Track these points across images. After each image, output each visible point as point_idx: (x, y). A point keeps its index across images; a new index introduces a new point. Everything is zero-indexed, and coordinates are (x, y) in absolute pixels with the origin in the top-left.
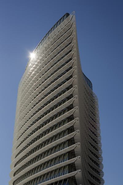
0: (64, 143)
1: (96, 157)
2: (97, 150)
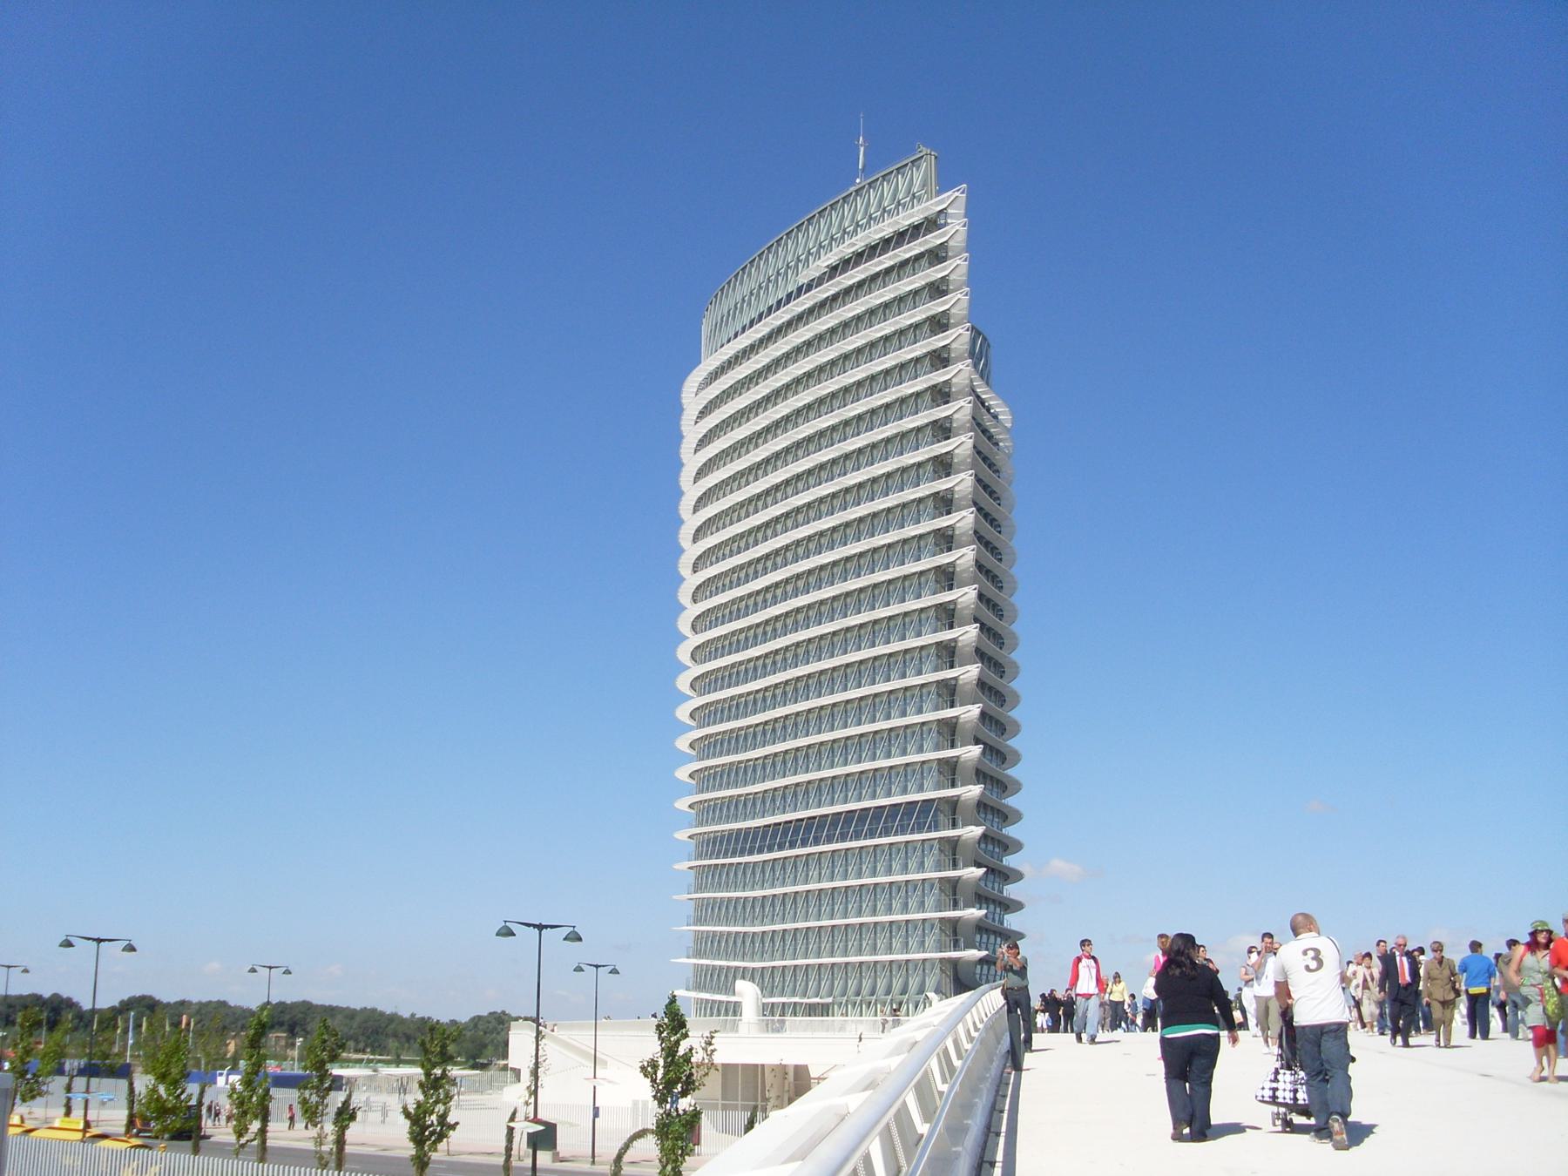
0: (916, 293)
1: (990, 467)
2: (997, 471)
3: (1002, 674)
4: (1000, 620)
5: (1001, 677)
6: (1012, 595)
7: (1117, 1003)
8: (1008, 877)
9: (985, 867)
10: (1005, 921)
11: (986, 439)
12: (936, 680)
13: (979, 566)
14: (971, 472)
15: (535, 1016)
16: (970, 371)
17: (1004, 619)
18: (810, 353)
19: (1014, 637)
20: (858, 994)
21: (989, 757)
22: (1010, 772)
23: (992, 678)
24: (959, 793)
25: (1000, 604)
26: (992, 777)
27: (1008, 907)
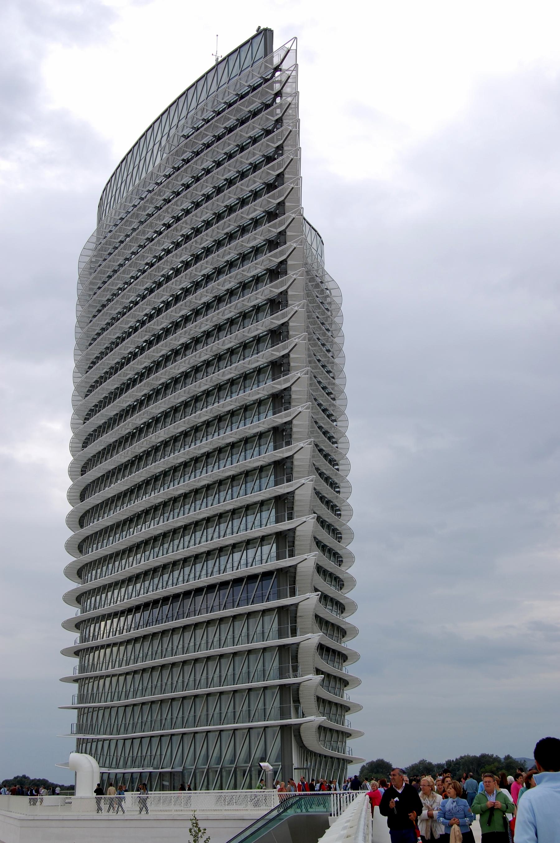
3: (339, 539)
4: (339, 542)
5: (340, 565)
6: (348, 498)
7: (443, 822)
8: (348, 684)
9: (323, 673)
10: (345, 695)
11: (326, 416)
12: (273, 460)
13: (319, 569)
14: (309, 440)
15: (77, 710)
16: (314, 521)
17: (343, 541)
18: (126, 448)
19: (351, 534)
20: (246, 762)
21: (331, 608)
22: (347, 620)
23: (330, 565)
24: (289, 419)
25: (337, 504)
26: (333, 624)
27: (351, 735)
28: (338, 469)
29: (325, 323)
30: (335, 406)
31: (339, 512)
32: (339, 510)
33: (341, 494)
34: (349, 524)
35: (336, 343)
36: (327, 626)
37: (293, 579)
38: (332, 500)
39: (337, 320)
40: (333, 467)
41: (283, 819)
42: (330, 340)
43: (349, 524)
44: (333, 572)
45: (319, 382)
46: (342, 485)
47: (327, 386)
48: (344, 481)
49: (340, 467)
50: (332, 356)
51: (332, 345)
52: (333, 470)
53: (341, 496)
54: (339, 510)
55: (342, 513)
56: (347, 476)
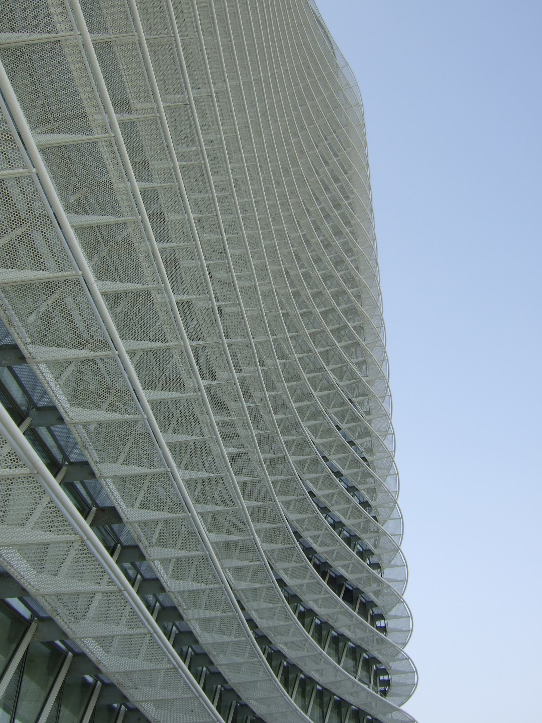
4: (384, 693)
28: (384, 629)
29: (359, 487)
30: (379, 582)
31: (386, 677)
32: (385, 672)
33: (389, 634)
34: (408, 650)
35: (385, 533)
36: (339, 714)
37: (233, 589)
38: (364, 646)
39: (388, 484)
40: (373, 623)
41: (361, 306)
42: (372, 527)
43: (408, 650)
44: (362, 707)
45: (337, 525)
46: (394, 665)
47: (358, 533)
48: (399, 656)
49: (390, 624)
50: (375, 518)
51: (373, 491)
52: (371, 631)
53: (390, 638)
54: (385, 672)
55: (394, 679)
56: (405, 644)
